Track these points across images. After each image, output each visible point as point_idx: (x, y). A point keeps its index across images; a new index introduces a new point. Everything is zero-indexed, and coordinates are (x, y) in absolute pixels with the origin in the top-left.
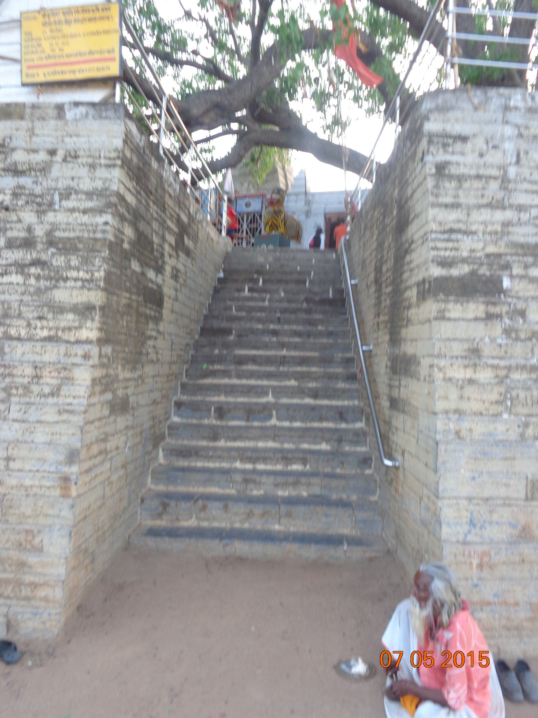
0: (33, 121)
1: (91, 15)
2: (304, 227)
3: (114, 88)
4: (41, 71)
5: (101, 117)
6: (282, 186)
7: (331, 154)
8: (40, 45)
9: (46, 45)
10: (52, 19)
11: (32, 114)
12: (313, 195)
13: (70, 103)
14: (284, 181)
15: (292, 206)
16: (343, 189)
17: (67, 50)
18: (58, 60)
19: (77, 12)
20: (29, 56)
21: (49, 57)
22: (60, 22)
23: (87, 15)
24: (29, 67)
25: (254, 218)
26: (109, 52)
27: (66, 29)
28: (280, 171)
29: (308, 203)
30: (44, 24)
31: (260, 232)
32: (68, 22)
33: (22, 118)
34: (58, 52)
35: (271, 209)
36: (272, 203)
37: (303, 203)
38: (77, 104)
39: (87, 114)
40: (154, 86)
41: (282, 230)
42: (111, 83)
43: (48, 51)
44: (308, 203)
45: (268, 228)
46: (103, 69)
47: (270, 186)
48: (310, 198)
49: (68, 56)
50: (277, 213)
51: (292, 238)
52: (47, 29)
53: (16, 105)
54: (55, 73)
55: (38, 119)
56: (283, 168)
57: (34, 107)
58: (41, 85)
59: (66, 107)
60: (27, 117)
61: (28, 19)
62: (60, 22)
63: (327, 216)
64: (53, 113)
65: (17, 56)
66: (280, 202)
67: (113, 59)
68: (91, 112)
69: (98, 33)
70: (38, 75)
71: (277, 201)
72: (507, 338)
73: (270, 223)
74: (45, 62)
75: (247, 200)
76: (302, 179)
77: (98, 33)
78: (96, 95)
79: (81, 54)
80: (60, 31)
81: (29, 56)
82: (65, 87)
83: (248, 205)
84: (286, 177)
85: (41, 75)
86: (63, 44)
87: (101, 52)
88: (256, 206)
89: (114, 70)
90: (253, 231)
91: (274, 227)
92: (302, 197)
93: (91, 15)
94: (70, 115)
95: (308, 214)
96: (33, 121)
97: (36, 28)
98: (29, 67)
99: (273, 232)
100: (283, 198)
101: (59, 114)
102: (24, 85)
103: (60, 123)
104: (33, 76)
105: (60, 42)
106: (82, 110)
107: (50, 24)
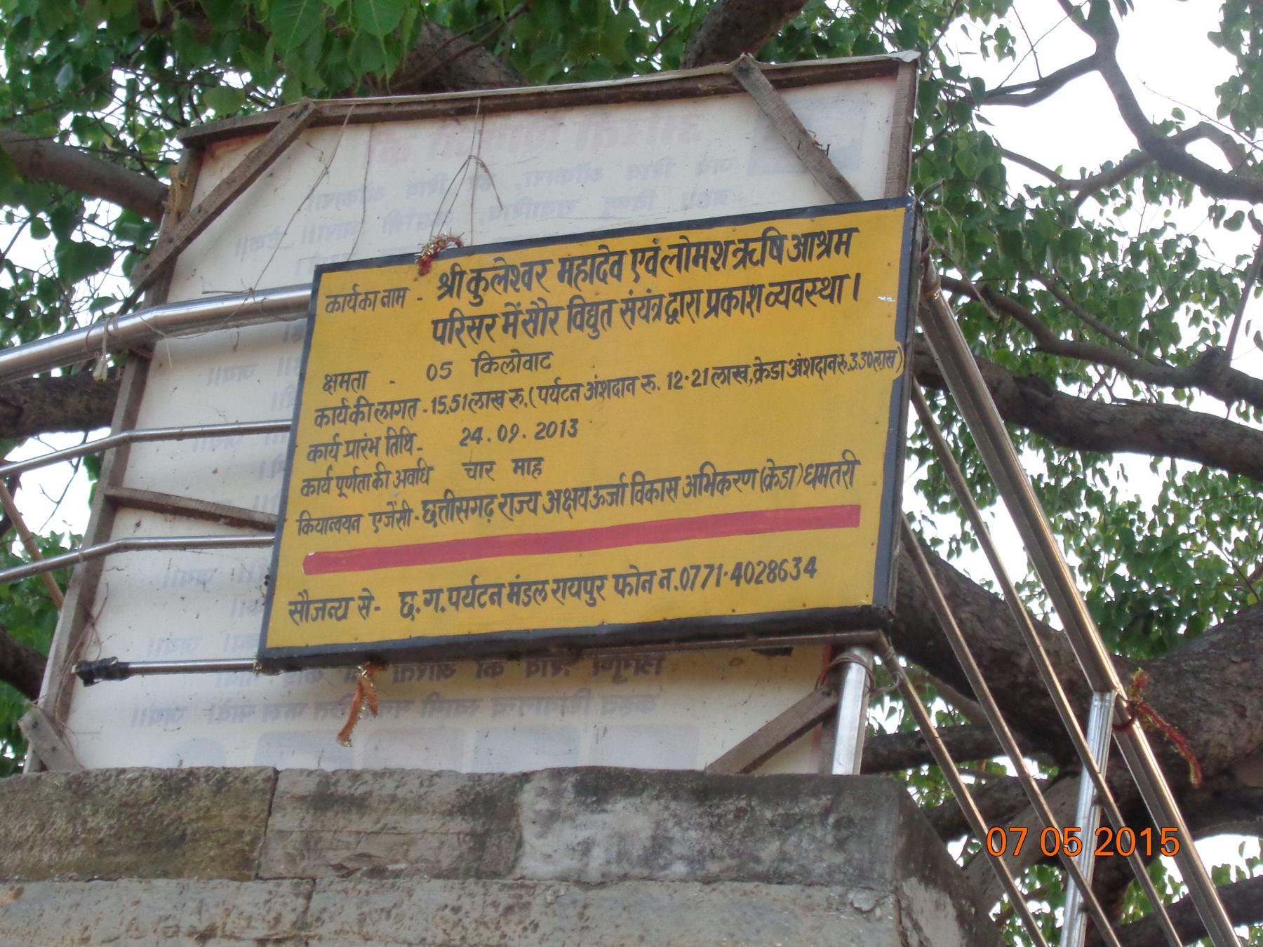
0: (308, 886)
1: (730, 277)
3: (833, 679)
4: (387, 584)
5: (747, 872)
8: (402, 441)
9: (437, 437)
10: (495, 301)
11: (310, 844)
13: (558, 774)
16: (1069, 19)
17: (564, 466)
18: (500, 526)
19: (650, 259)
20: (328, 504)
21: (451, 505)
22: (541, 318)
23: (702, 278)
24: (320, 563)
26: (820, 474)
27: (574, 355)
30: (444, 329)
32: (586, 316)
33: (244, 866)
34: (505, 481)
38: (600, 785)
39: (659, 844)
40: (1043, 628)
42: (813, 655)
43: (448, 475)
46: (774, 571)
49: (565, 499)
52: (460, 353)
53: (223, 781)
54: (469, 594)
55: (344, 872)
57: (328, 797)
58: (376, 657)
59: (531, 802)
60: (276, 857)
61: (357, 300)
62: (541, 318)
64: (439, 837)
65: (259, 498)
67: (847, 516)
68: (689, 836)
69: (765, 370)
70: (367, 601)
74: (418, 533)
77: (765, 370)
78: (703, 727)
79: (644, 489)
80: (535, 360)
81: (328, 504)
82: (514, 669)
85: (388, 600)
86: (545, 431)
87: (773, 476)
89: (845, 574)
93: (730, 277)
94: (544, 852)
96: (308, 886)
97: (395, 350)
98: (320, 563)
101: (479, 841)
102: (271, 662)
103: (478, 900)
104: (336, 608)
105: (527, 418)
106: (631, 819)
107: (480, 325)
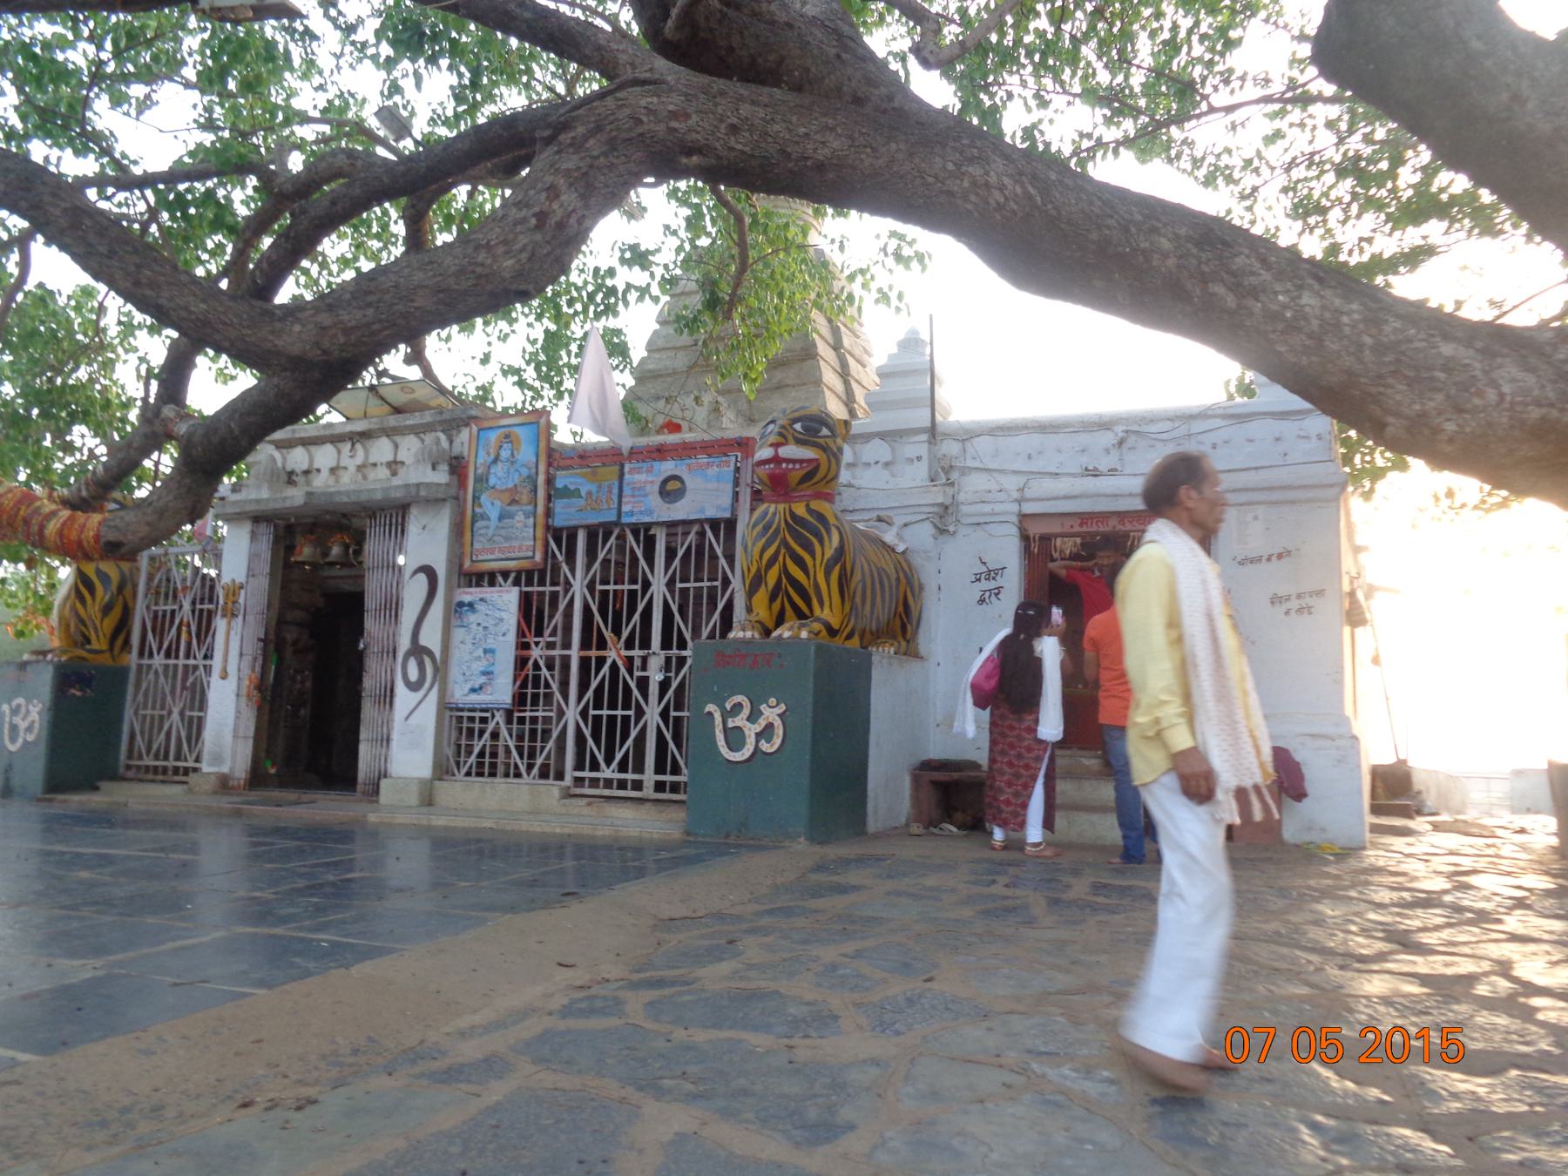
2: (928, 575)
6: (836, 409)
7: (1064, 237)
12: (967, 435)
14: (839, 386)
15: (877, 490)
25: (702, 546)
28: (823, 349)
29: (944, 472)
31: (727, 622)
35: (774, 510)
36: (778, 483)
37: (921, 472)
41: (829, 613)
44: (944, 472)
45: (762, 596)
47: (783, 405)
48: (950, 448)
50: (806, 531)
51: (875, 636)
56: (837, 346)
63: (1036, 530)
66: (817, 479)
71: (799, 474)
72: (363, 120)
73: (772, 577)
75: (668, 467)
76: (915, 370)
83: (671, 490)
84: (844, 374)
88: (708, 493)
90: (609, 733)
91: (792, 600)
92: (917, 447)
95: (944, 519)
99: (785, 632)
100: (835, 456)
